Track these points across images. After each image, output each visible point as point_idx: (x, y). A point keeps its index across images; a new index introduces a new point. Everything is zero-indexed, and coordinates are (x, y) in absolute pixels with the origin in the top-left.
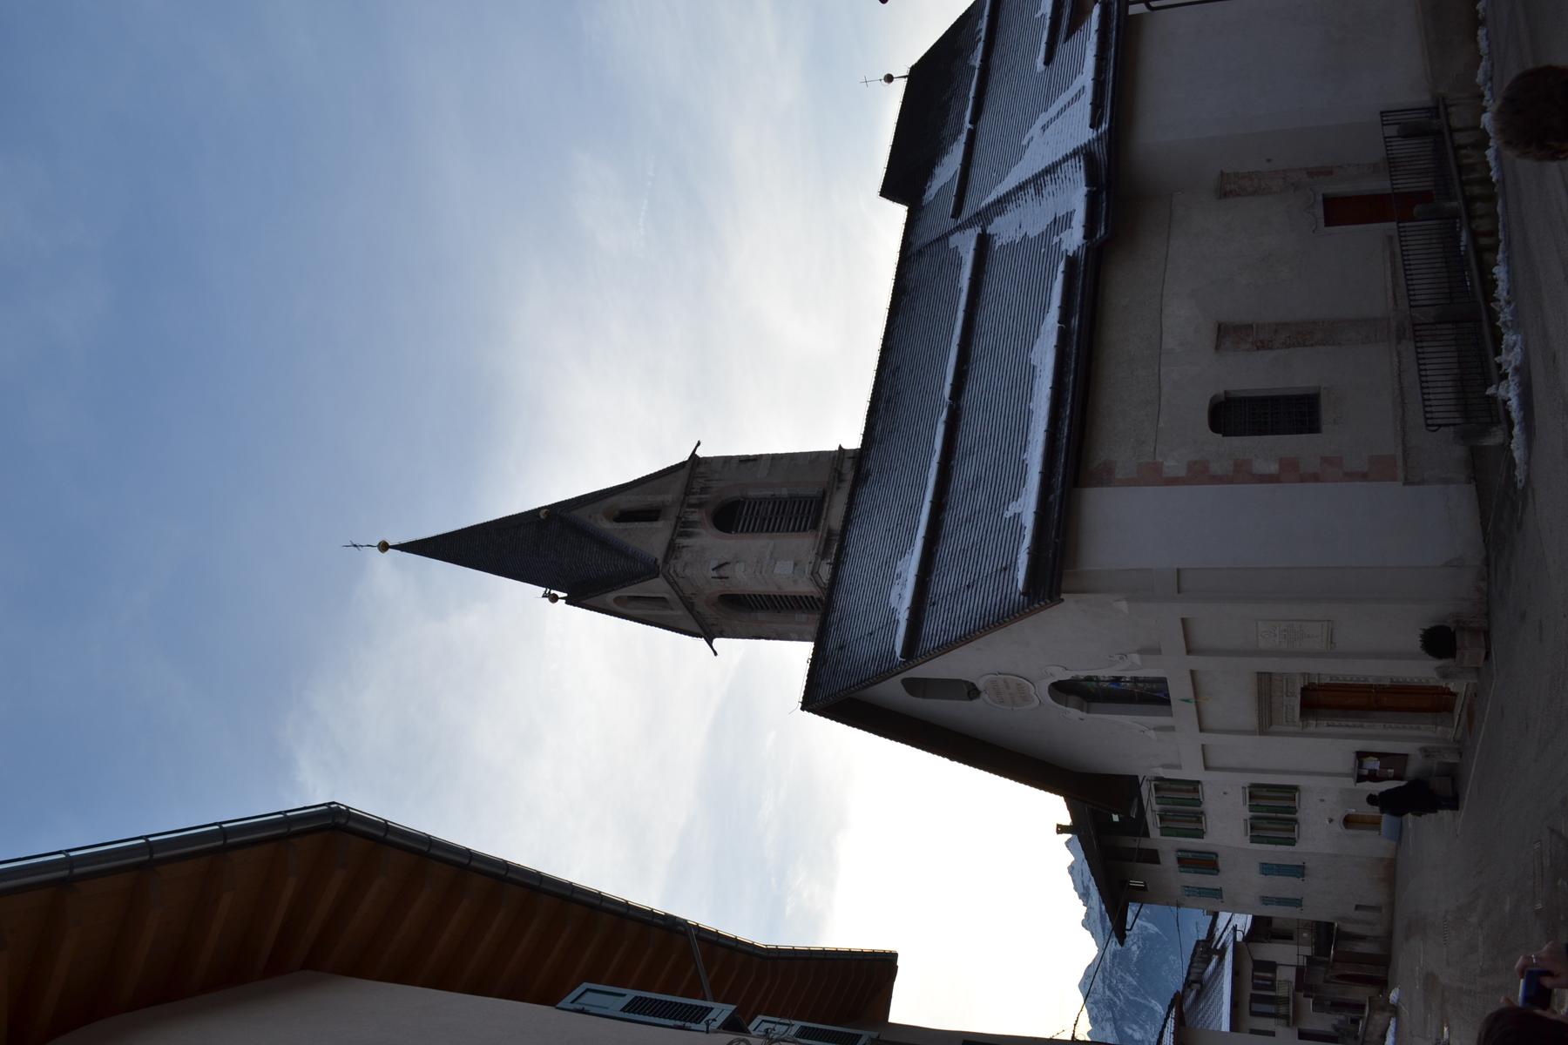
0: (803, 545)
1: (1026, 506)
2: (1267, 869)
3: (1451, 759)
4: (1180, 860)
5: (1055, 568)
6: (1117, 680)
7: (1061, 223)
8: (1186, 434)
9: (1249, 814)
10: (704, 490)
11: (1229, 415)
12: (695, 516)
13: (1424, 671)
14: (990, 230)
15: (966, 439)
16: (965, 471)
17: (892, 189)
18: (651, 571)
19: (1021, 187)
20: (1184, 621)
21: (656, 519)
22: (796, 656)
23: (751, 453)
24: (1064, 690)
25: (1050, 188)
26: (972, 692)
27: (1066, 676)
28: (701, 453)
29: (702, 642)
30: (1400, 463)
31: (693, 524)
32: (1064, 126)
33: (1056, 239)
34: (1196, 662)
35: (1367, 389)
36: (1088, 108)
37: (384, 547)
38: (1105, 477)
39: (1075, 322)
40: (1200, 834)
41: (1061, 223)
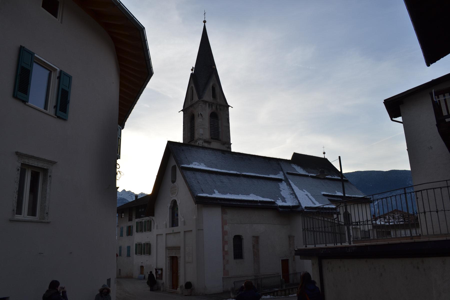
0: (207, 136)
1: (217, 195)
2: (129, 248)
3: (162, 289)
4: (130, 226)
5: (203, 202)
6: (177, 215)
7: (284, 200)
9: (143, 243)
10: (220, 109)
11: (238, 240)
12: (214, 108)
13: (182, 282)
14: (283, 182)
15: (233, 179)
16: (225, 179)
17: (295, 155)
18: (200, 97)
19: (293, 190)
20: (192, 231)
21: (213, 97)
22: (179, 138)
23: (230, 121)
24: (174, 205)
25: (292, 197)
26: (173, 182)
27: (178, 203)
28: (230, 108)
29: (182, 109)
30: (227, 276)
31: (212, 107)
32: (306, 199)
33: (280, 199)
34: (182, 233)
35: (244, 270)
36: (310, 206)
37: (205, 22)
38: (223, 212)
39: (259, 204)
40: (137, 231)
41: (284, 200)
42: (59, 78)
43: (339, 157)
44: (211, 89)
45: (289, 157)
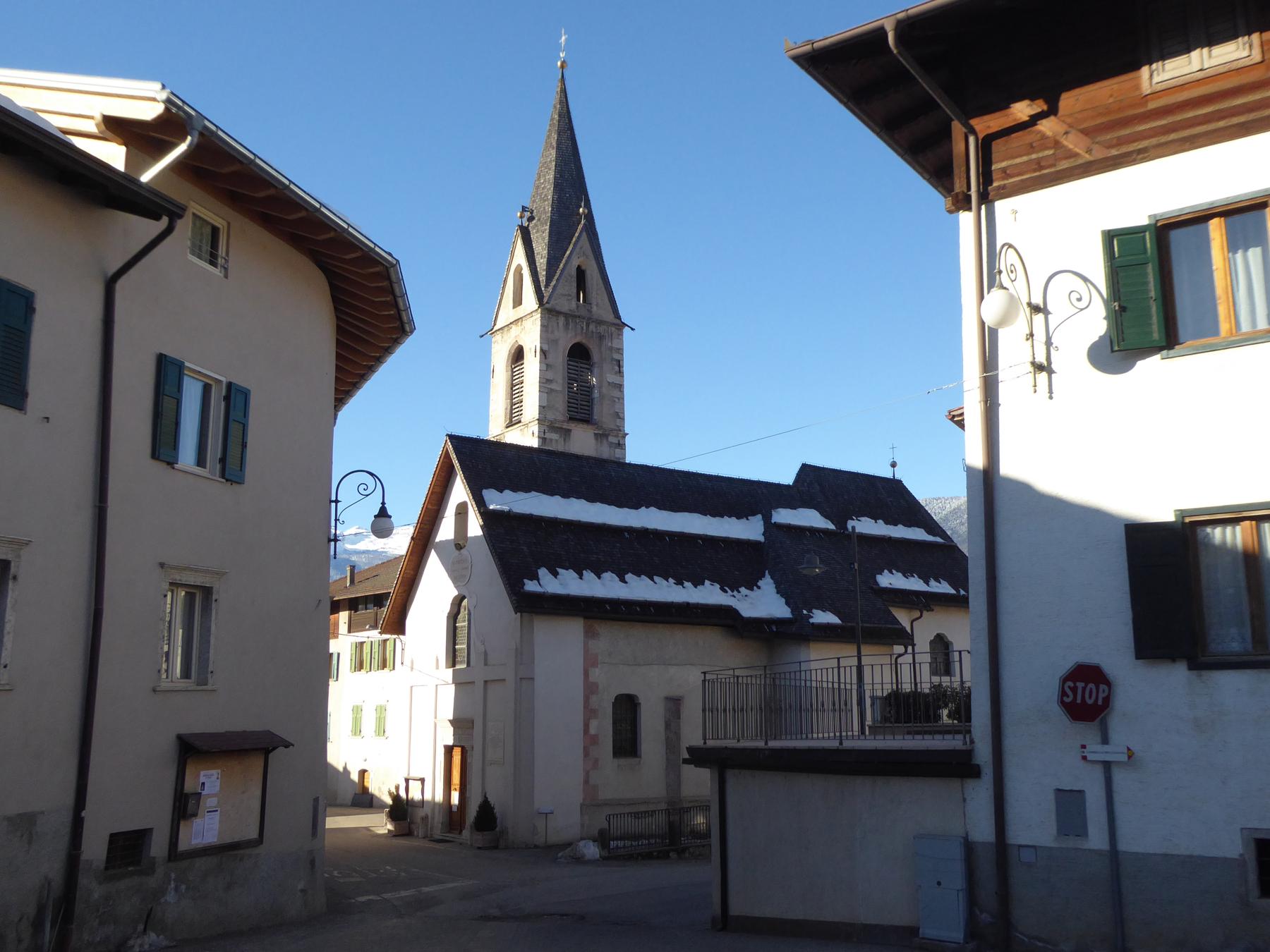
8: (613, 683)
22: (451, 743)
28: (626, 330)
38: (590, 634)
42: (227, 398)
43: (1051, 398)
44: (574, 272)
45: (787, 477)
